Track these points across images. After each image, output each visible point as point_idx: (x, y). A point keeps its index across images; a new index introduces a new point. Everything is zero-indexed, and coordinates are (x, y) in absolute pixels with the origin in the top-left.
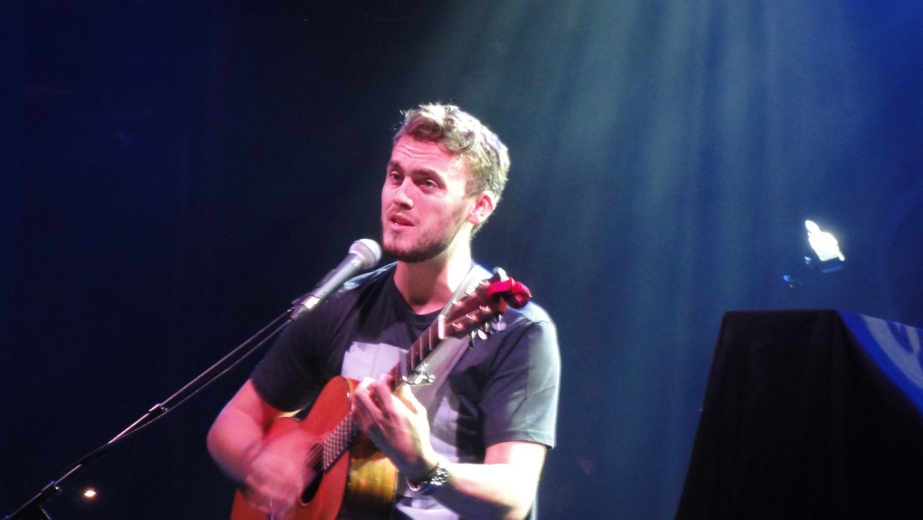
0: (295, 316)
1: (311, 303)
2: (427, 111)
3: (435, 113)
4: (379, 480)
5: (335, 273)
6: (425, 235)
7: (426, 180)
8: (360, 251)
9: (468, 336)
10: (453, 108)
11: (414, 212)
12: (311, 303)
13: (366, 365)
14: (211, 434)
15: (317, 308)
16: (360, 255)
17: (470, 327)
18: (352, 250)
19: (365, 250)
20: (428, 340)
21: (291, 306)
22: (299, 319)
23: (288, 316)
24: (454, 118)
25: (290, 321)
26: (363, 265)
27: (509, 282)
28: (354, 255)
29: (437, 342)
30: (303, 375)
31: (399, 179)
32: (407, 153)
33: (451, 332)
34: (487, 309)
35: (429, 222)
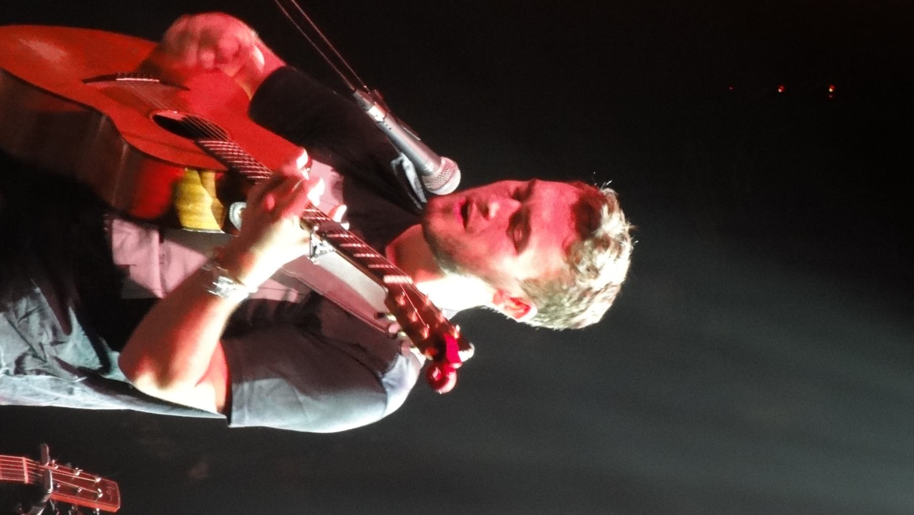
0: (358, 94)
1: (376, 113)
2: (611, 211)
3: (614, 224)
4: (190, 207)
5: (415, 140)
6: (458, 242)
7: (519, 229)
8: (445, 169)
9: (388, 311)
10: (628, 247)
11: (483, 223)
12: (376, 113)
13: (318, 183)
14: (241, 23)
15: (369, 120)
16: (440, 170)
17: (402, 314)
18: (444, 160)
19: (446, 177)
20: (374, 263)
21: (371, 89)
22: (355, 100)
23: (359, 87)
24: (609, 250)
25: (353, 88)
26: (427, 174)
27: (457, 360)
28: (439, 162)
29: (378, 275)
30: (299, 111)
31: (518, 196)
32: (552, 198)
33: (393, 291)
34: (426, 335)
35: (477, 246)
